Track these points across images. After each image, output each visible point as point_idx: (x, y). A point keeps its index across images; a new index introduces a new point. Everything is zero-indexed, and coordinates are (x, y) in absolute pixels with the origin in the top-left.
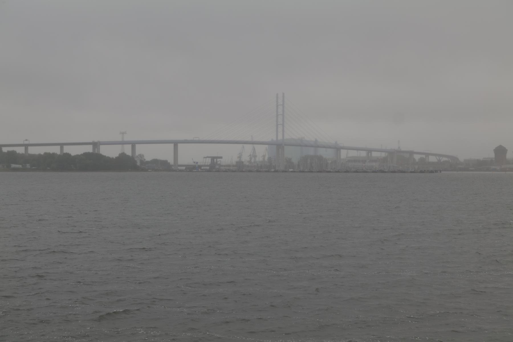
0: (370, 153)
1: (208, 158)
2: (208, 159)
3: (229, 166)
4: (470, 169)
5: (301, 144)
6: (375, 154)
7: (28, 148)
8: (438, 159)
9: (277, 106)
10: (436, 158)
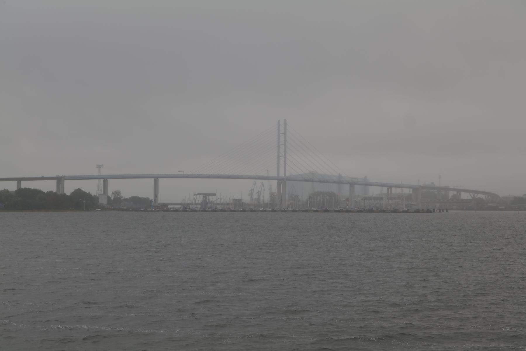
0: (389, 190)
1: (199, 195)
2: (198, 196)
3: (227, 204)
4: (500, 207)
6: (394, 191)
7: (21, 182)
9: (279, 134)
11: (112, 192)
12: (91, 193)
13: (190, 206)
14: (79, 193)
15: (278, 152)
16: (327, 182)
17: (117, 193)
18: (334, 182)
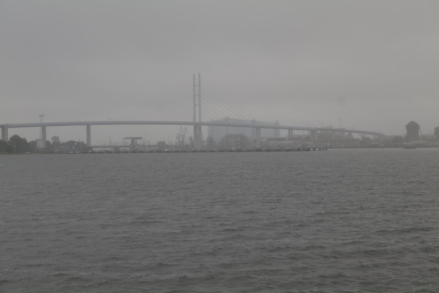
1: (128, 139)
2: (127, 139)
5: (226, 124)
6: (296, 133)
8: (362, 136)
10: (360, 135)
11: (52, 137)
12: (26, 139)
13: (120, 148)
14: (16, 138)
15: (194, 101)
16: (243, 126)
17: (55, 138)
18: (249, 126)
